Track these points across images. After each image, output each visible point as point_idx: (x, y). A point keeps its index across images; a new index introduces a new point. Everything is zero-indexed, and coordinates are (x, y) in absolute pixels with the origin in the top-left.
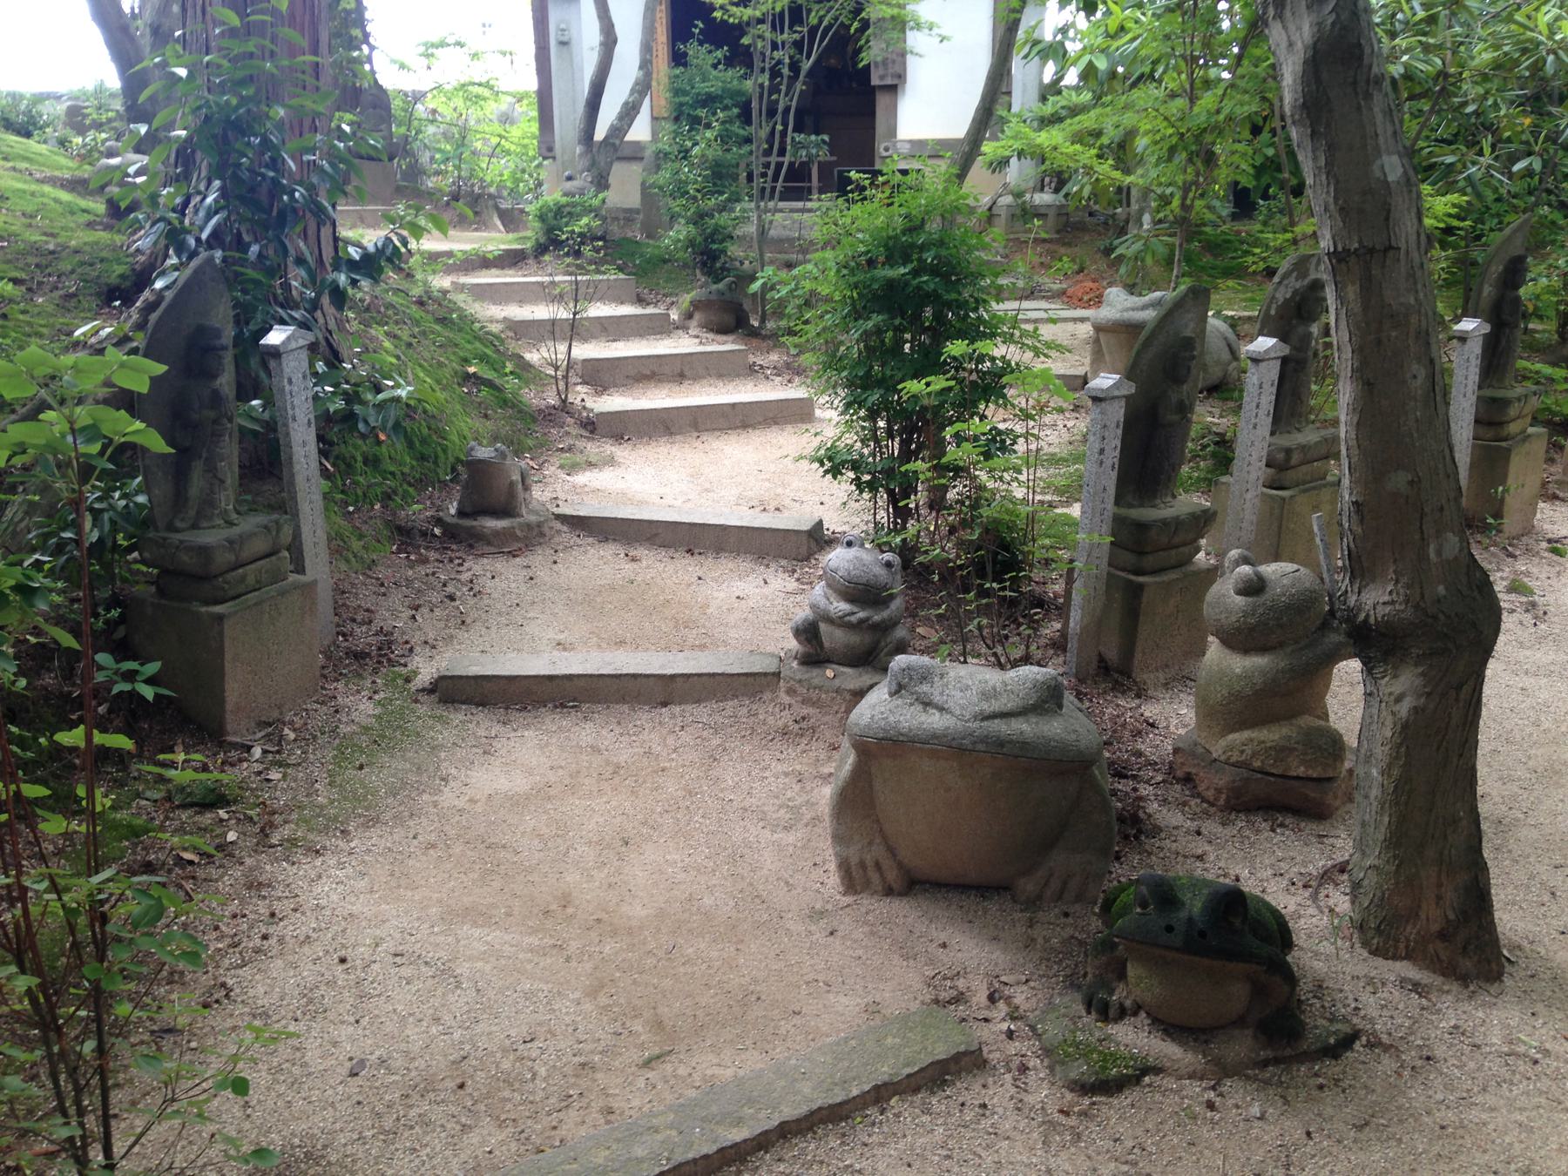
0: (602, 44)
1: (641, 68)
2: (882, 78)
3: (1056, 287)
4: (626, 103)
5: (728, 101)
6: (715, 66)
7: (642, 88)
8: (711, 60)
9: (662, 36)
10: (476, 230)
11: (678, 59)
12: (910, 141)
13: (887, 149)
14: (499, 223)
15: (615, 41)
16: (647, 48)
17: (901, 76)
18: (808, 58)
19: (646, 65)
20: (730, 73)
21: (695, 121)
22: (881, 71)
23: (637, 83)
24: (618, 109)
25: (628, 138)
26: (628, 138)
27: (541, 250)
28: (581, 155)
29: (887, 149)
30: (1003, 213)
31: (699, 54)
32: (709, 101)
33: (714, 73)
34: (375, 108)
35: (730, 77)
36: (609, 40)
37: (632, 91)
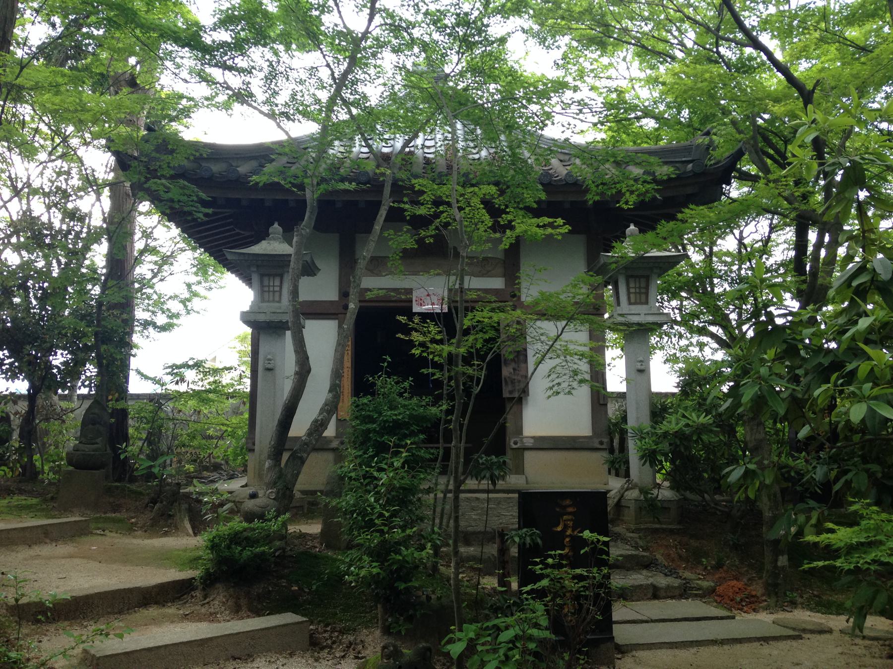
0: (296, 373)
1: (330, 391)
2: (511, 392)
3: (705, 584)
4: (316, 421)
5: (414, 428)
6: (401, 395)
7: (330, 408)
8: (397, 389)
9: (348, 363)
10: (166, 534)
11: (361, 387)
12: (533, 437)
13: (515, 443)
14: (188, 526)
15: (309, 371)
16: (337, 374)
17: (525, 391)
18: (478, 385)
19: (335, 388)
20: (415, 400)
21: (382, 448)
22: (510, 388)
23: (326, 404)
24: (308, 426)
25: (324, 435)
26: (324, 435)
27: (209, 581)
28: (269, 469)
29: (515, 443)
30: (632, 506)
31: (386, 384)
32: (395, 428)
33: (400, 400)
34: (93, 424)
35: (416, 405)
36: (304, 370)
37: (322, 410)
